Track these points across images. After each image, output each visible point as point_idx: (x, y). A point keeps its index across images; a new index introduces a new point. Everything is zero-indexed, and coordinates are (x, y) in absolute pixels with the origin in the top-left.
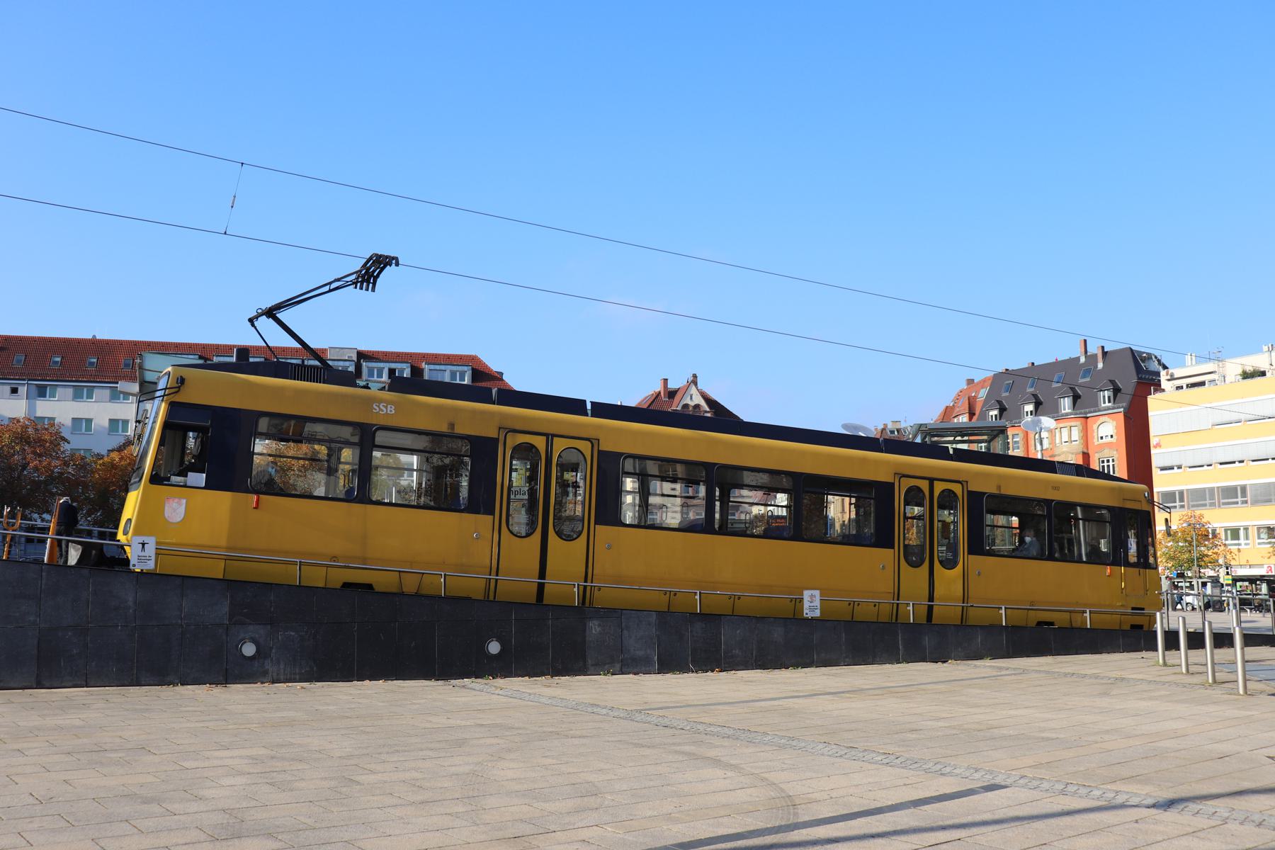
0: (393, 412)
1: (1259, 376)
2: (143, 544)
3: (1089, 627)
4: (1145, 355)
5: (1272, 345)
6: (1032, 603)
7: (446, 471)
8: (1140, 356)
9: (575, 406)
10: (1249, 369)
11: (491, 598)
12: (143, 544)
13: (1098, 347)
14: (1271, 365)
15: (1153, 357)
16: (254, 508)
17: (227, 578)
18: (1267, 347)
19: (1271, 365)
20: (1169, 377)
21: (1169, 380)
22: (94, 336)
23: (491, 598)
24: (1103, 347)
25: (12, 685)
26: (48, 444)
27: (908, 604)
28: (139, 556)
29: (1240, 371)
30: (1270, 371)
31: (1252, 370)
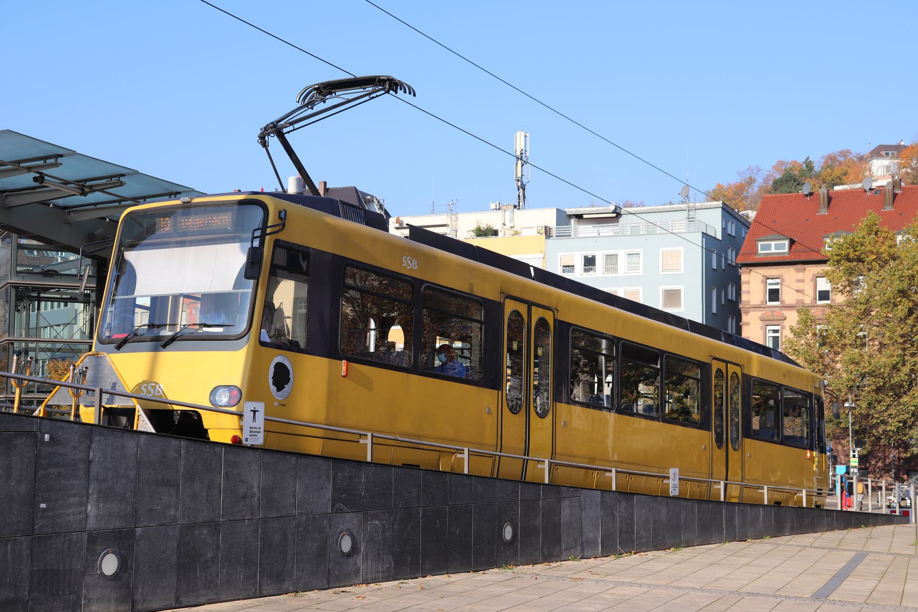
0: (416, 268)
1: (492, 235)
2: (255, 412)
3: (805, 505)
4: (369, 197)
5: (499, 203)
6: (592, 460)
7: (462, 339)
8: (364, 198)
9: (520, 268)
10: (483, 226)
11: (495, 476)
12: (255, 412)
13: (320, 183)
14: (504, 224)
15: (375, 200)
16: (343, 376)
17: (375, 462)
18: (494, 204)
19: (504, 224)
20: (398, 225)
21: (397, 228)
22: (719, 185)
23: (495, 476)
24: (325, 183)
25: (763, 238)
26: (406, 310)
27: (462, 452)
28: (251, 428)
29: (474, 227)
30: (503, 231)
31: (486, 227)
